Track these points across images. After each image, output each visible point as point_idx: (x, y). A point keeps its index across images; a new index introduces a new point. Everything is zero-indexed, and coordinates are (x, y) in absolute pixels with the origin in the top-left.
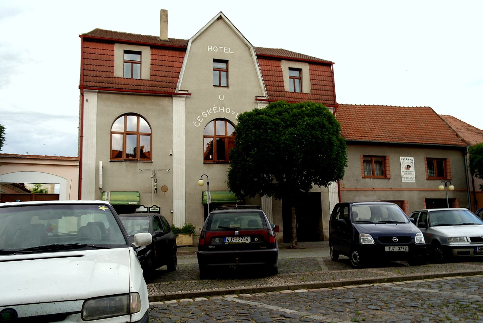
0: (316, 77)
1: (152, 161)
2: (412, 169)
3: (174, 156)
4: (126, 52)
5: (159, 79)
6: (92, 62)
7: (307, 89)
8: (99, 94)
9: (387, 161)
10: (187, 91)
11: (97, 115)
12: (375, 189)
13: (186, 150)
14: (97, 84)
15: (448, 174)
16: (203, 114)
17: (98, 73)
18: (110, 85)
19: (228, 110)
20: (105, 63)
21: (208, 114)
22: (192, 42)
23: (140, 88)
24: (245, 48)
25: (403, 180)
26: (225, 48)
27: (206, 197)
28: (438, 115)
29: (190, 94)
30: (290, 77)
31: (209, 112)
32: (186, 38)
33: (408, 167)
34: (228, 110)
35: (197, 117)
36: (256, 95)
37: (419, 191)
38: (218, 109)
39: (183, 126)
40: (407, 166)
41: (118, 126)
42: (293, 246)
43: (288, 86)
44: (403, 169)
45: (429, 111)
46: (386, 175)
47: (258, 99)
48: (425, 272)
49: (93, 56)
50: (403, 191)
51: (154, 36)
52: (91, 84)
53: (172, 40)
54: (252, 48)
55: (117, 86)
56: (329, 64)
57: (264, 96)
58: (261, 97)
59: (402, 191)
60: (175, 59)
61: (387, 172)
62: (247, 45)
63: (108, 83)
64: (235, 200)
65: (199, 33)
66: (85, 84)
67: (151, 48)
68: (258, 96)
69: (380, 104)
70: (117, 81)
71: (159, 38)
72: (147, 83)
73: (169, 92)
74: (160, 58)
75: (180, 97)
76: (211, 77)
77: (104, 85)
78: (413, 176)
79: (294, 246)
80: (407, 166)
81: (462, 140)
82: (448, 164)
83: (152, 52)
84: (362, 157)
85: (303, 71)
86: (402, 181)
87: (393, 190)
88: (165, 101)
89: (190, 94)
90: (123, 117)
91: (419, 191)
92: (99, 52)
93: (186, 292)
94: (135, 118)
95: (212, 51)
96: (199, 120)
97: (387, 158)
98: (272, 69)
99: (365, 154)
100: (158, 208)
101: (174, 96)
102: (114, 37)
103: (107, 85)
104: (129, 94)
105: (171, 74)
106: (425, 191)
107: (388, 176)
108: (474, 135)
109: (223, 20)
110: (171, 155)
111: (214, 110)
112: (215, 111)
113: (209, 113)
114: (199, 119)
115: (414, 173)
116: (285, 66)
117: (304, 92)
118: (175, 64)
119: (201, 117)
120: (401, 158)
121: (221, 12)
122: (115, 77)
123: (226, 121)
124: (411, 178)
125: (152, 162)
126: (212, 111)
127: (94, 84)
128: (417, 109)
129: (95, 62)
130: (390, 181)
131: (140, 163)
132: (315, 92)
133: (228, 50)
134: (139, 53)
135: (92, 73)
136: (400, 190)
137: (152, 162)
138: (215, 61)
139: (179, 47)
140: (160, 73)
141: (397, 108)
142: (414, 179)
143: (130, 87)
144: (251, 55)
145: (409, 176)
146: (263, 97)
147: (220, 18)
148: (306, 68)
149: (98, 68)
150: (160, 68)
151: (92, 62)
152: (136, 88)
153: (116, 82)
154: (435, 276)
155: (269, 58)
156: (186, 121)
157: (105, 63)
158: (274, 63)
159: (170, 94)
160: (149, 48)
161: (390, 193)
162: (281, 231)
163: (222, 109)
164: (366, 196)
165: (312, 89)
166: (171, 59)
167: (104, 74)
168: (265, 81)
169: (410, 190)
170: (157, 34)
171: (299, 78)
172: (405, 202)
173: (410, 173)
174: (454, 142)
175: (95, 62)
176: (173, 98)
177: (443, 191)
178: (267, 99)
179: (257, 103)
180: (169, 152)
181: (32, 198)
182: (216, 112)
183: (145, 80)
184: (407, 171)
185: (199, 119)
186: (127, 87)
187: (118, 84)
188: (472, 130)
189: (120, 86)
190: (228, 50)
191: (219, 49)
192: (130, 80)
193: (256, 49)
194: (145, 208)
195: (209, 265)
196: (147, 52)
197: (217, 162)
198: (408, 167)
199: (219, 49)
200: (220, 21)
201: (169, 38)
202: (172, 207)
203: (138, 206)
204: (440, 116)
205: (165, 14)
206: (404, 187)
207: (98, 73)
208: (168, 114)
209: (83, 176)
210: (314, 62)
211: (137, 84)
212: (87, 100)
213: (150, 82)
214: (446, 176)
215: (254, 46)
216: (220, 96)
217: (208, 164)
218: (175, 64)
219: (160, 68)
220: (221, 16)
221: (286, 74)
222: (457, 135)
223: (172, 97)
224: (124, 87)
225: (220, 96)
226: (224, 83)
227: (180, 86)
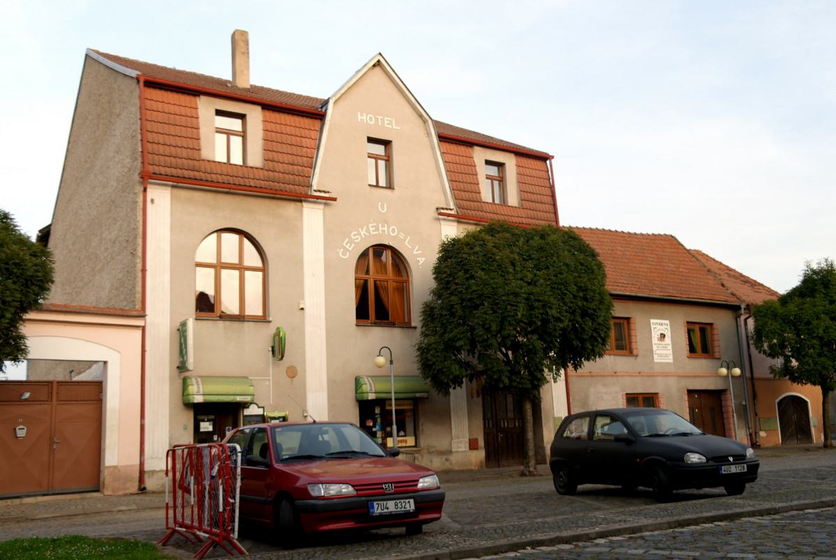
0: (528, 180)
1: (271, 319)
2: (668, 340)
3: (307, 311)
4: (219, 113)
5: (280, 167)
6: (161, 128)
7: (513, 199)
8: (176, 191)
9: (632, 326)
10: (328, 192)
11: (171, 230)
12: (617, 374)
13: (327, 301)
14: (174, 172)
15: (717, 349)
16: (354, 235)
17: (173, 150)
18: (197, 175)
19: (393, 231)
20: (183, 132)
21: (360, 235)
22: (335, 102)
23: (249, 182)
24: (419, 121)
25: (657, 359)
26: (386, 118)
27: (366, 388)
28: (688, 250)
29: (335, 199)
30: (488, 177)
31: (364, 232)
32: (322, 95)
33: (663, 336)
34: (393, 231)
35: (344, 240)
36: (437, 206)
37: (679, 376)
38: (377, 229)
39: (322, 256)
40: (661, 334)
41: (206, 250)
42: (530, 472)
43: (486, 192)
44: (655, 340)
45: (671, 241)
46: (630, 349)
47: (442, 213)
48: (657, 518)
49: (161, 117)
50: (656, 376)
51: (218, 79)
52: (163, 170)
53: (254, 89)
54: (430, 121)
55: (209, 177)
56: (543, 158)
57: (452, 207)
58: (447, 209)
59: (654, 376)
60: (304, 132)
61: (634, 346)
62: (422, 116)
63: (277, 182)
64: (413, 392)
65: (346, 88)
66: (151, 169)
67: (263, 108)
68: (443, 209)
69: (600, 227)
70: (208, 167)
71: (229, 82)
72: (262, 174)
73: (298, 192)
74: (278, 128)
75: (314, 202)
76: (370, 171)
77: (186, 174)
78: (669, 351)
79: (532, 472)
80: (661, 334)
81: (732, 294)
82: (715, 332)
83: (264, 116)
84: (686, 324)
85: (249, 119)
86: (655, 361)
87: (642, 376)
88: (289, 209)
89: (335, 199)
90: (215, 235)
91: (679, 376)
92: (172, 109)
93: (807, 502)
94: (235, 237)
95: (365, 122)
96: (347, 247)
97: (632, 321)
98: (460, 161)
99: (690, 320)
100: (262, 409)
101: (305, 201)
102: (471, 138)
103: (192, 174)
104: (227, 193)
105: (300, 160)
106: (686, 376)
107: (635, 352)
108: (739, 285)
109: (381, 67)
110: (302, 309)
111: (371, 229)
112: (373, 231)
113: (362, 234)
114: (346, 244)
115: (670, 347)
116: (480, 156)
117: (510, 204)
118: (305, 142)
119: (351, 242)
120: (652, 321)
121: (380, 54)
122: (203, 160)
123: (243, 236)
124: (666, 356)
125: (270, 322)
126: (368, 230)
127: (169, 171)
128: (622, 235)
129: (166, 129)
130: (638, 359)
131: (250, 323)
132: (526, 204)
133: (390, 123)
134: (242, 117)
135: (161, 149)
136: (651, 376)
137: (270, 322)
138: (371, 140)
139: (314, 113)
140: (280, 157)
141: (625, 235)
142: (671, 357)
143: (231, 180)
144: (429, 134)
145: (664, 352)
146: (451, 210)
147: (378, 64)
148: (510, 161)
149: (172, 141)
150: (280, 147)
151: (161, 128)
152: (241, 181)
153: (205, 168)
154: (537, 543)
155: (454, 140)
156: (326, 247)
157: (183, 132)
158: (462, 150)
159: (300, 198)
160: (259, 108)
161: (638, 380)
162: (481, 448)
163: (384, 227)
164: (605, 385)
165: (522, 200)
166: (298, 132)
167: (184, 153)
168: (451, 181)
169: (666, 375)
170: (226, 75)
171: (242, 134)
172: (660, 396)
173: (665, 347)
174: (721, 298)
175: (166, 129)
176: (305, 204)
177: (739, 377)
178: (456, 213)
179: (439, 219)
180: (299, 303)
181: (52, 390)
182: (375, 233)
183: (512, 207)
184: (661, 343)
185: (346, 244)
186: (226, 179)
187: (210, 173)
188: (734, 277)
189: (214, 177)
190: (390, 123)
191: (377, 120)
192: (225, 165)
193: (437, 124)
194: (259, 407)
195: (620, 487)
196: (255, 115)
197: (375, 324)
198: (663, 336)
199: (377, 120)
200: (377, 69)
201: (251, 86)
202: (305, 406)
203: (245, 405)
204: (692, 252)
205: (243, 38)
206: (657, 370)
207: (173, 150)
208: (294, 231)
209: (147, 348)
210: (521, 153)
211: (211, 170)
212: (152, 201)
213: (266, 173)
214: (713, 353)
215: (434, 118)
216: (380, 204)
217: (363, 327)
218: (305, 142)
219: (280, 147)
220: (379, 61)
221: (483, 171)
222: (723, 285)
223: (301, 201)
224: (220, 179)
225: (380, 204)
226: (382, 182)
227: (317, 182)
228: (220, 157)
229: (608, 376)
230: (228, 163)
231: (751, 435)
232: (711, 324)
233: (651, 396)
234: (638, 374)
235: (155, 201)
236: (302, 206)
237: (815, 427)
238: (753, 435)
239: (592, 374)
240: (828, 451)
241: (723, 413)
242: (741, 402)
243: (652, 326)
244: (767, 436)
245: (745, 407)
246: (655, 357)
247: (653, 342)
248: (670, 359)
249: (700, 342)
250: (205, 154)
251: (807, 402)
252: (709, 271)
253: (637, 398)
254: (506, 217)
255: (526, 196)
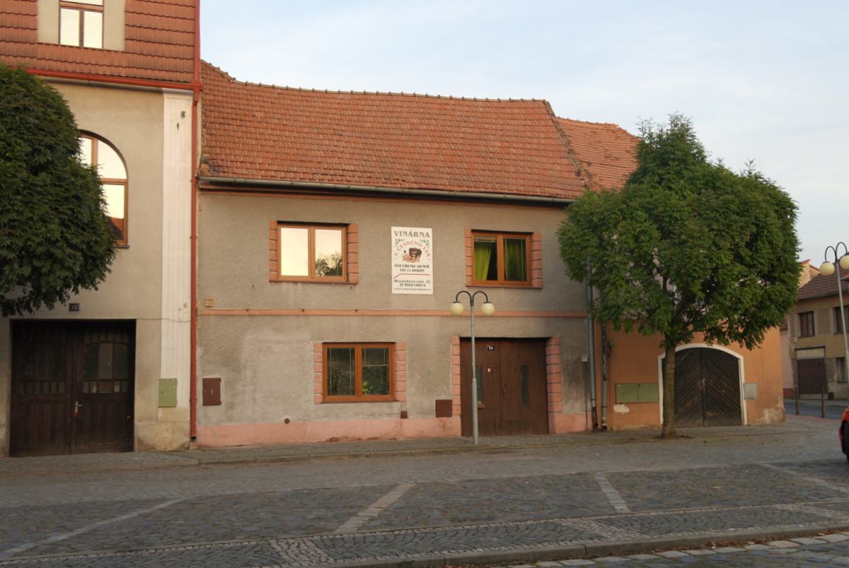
2: (426, 259)
15: (535, 274)
25: (396, 289)
33: (415, 253)
40: (411, 250)
44: (398, 257)
86: (394, 292)
115: (430, 271)
120: (394, 229)
123: (95, 140)
132: (138, 47)
142: (430, 286)
161: (354, 322)
172: (398, 347)
214: (531, 280)
228: (69, 37)
229: (289, 315)
230: (81, 47)
231: (594, 410)
232: (530, 234)
233: (385, 347)
234: (353, 313)
235: (180, 115)
236: (163, 98)
237: (749, 399)
238: (598, 410)
239: (250, 312)
240: (671, 444)
241: (546, 374)
242: (579, 358)
243: (394, 237)
244: (631, 412)
245: (586, 365)
246: (395, 285)
247: (394, 262)
248: (429, 289)
249: (503, 262)
250: (45, 33)
251: (736, 360)
252: (571, 151)
253: (353, 351)
254: (23, 61)
255: (137, 33)
